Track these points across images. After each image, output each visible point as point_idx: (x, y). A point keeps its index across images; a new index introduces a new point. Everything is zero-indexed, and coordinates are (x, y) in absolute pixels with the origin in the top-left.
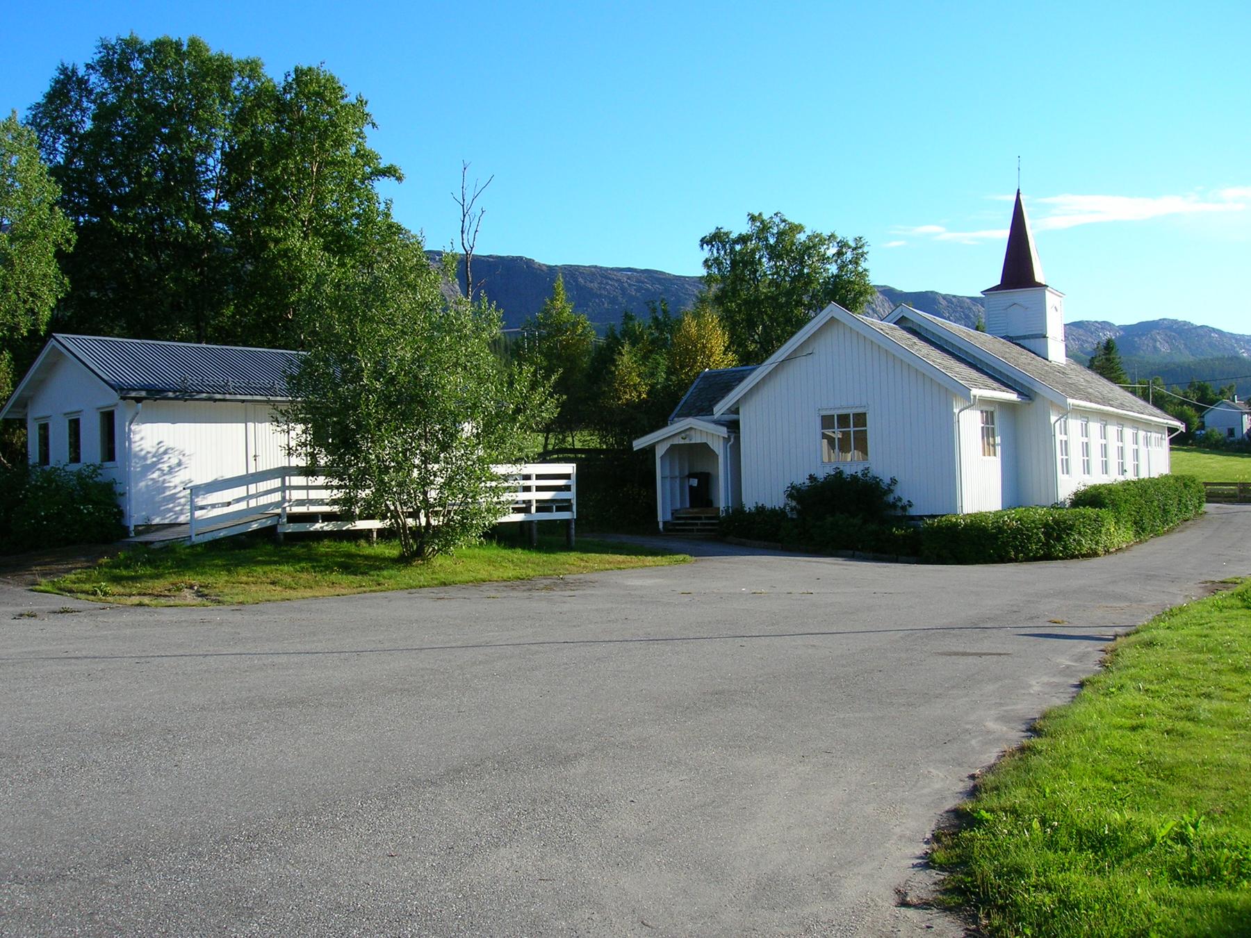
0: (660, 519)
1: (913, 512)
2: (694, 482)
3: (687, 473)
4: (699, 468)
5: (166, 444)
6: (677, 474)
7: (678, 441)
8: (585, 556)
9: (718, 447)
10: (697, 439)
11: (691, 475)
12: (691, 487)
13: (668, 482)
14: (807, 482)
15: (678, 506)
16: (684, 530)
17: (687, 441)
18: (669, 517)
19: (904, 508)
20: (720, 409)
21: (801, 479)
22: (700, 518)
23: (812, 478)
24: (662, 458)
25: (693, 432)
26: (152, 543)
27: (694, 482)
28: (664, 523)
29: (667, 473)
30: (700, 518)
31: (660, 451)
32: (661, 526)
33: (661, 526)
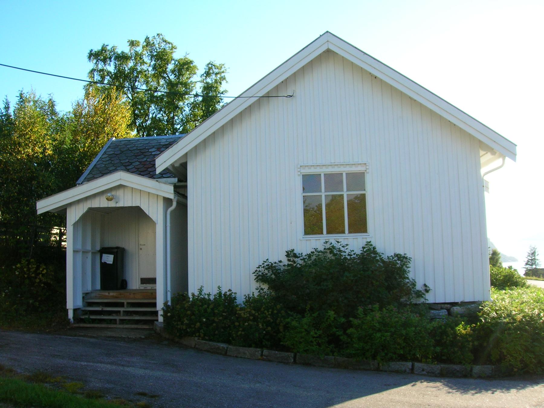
0: (70, 305)
1: (430, 298)
2: (109, 259)
3: (98, 248)
4: (112, 243)
5: (106, 44)
6: (89, 248)
7: (102, 203)
8: (281, 353)
9: (156, 212)
10: (126, 200)
11: (104, 250)
12: (104, 265)
13: (80, 256)
14: (285, 261)
15: (89, 288)
16: (101, 321)
17: (112, 204)
18: (80, 303)
19: (419, 294)
20: (163, 162)
21: (278, 256)
22: (122, 305)
23: (291, 254)
24: (75, 225)
25: (120, 193)
26: (166, 304)
27: (109, 259)
28: (75, 310)
29: (79, 247)
30: (122, 305)
31: (73, 216)
32: (71, 315)
33: (71, 315)
